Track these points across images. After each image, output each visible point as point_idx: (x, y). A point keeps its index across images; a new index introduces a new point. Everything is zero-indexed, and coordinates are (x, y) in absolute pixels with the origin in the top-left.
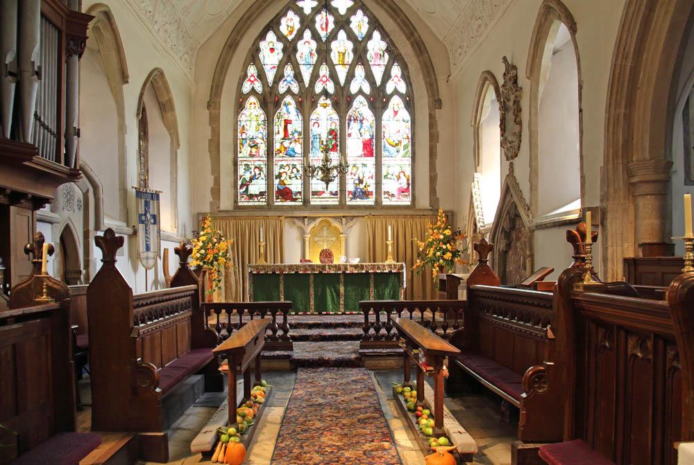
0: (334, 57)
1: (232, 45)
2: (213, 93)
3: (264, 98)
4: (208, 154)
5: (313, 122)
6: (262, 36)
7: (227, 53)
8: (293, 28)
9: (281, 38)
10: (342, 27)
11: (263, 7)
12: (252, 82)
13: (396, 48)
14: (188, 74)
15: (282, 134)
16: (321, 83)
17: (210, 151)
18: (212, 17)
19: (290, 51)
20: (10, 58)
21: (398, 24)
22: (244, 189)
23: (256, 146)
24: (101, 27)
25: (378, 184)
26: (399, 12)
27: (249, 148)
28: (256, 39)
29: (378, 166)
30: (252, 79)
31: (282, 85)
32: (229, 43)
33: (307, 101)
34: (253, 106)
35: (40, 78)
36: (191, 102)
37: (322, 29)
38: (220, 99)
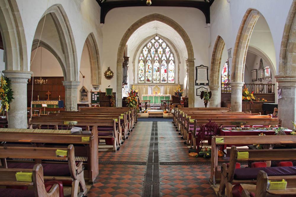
0: (159, 52)
1: (137, 50)
6: (144, 48)
9: (147, 48)
15: (148, 68)
19: (149, 51)
25: (167, 79)
29: (168, 75)
33: (153, 61)
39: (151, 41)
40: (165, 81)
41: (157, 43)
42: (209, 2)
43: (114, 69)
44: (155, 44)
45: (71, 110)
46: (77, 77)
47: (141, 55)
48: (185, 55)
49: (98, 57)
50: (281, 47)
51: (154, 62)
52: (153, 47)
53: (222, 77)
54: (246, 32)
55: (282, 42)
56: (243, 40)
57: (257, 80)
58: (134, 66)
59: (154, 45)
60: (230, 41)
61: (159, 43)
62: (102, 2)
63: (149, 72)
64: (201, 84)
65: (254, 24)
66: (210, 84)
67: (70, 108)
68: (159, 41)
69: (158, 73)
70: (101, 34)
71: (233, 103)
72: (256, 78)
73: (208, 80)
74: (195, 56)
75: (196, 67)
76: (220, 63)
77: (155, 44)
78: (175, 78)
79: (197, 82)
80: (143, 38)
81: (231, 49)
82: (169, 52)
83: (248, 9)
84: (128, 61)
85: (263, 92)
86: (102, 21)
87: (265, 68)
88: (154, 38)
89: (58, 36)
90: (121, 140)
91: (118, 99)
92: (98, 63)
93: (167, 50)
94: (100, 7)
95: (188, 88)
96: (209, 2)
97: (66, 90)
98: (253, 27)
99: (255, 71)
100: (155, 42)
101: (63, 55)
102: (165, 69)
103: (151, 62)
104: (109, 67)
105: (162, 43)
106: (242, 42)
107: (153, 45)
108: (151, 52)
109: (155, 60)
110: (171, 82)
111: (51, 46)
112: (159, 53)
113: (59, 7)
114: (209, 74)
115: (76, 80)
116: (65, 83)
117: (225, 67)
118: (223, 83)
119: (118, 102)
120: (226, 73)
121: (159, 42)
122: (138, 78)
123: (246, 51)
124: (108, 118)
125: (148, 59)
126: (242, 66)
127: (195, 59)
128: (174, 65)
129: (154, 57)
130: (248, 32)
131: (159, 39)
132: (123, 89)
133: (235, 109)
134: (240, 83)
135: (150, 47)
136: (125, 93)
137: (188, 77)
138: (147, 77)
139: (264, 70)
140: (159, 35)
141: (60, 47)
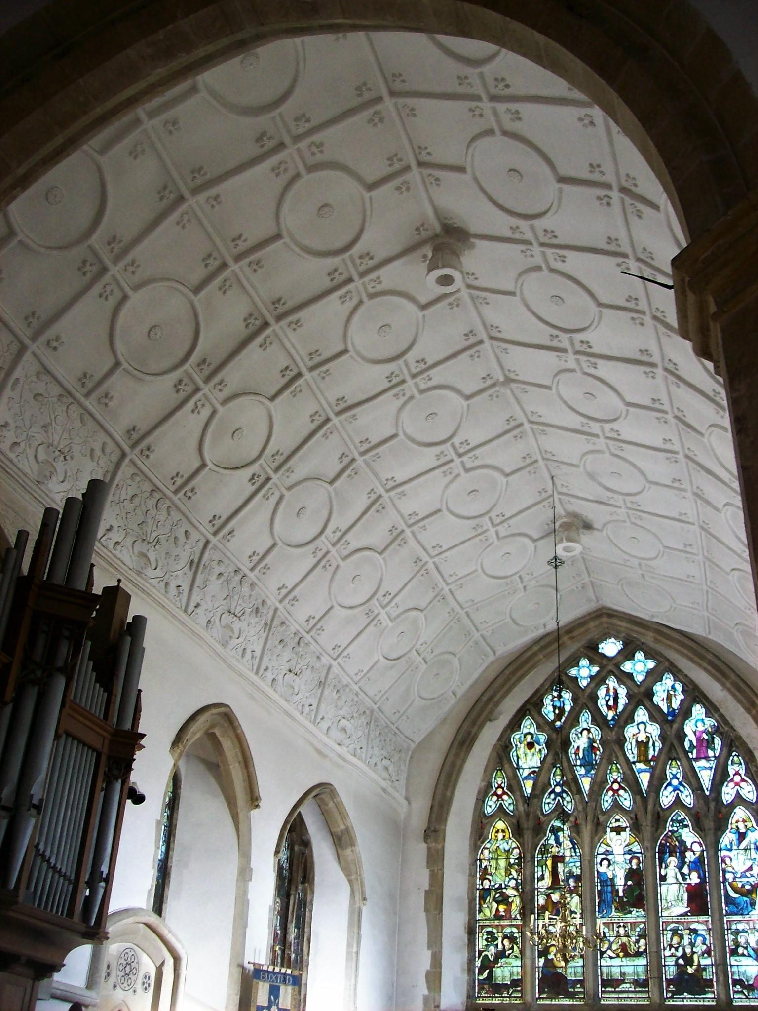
0: (631, 751)
1: (463, 742)
2: (434, 815)
3: (518, 822)
4: (423, 915)
5: (600, 857)
6: (515, 725)
7: (457, 755)
8: (562, 710)
9: (543, 724)
10: (585, 706)
11: (512, 682)
12: (499, 797)
13: (732, 728)
14: (390, 790)
15: (548, 881)
16: (495, 798)
17: (427, 910)
18: (429, 702)
19: (558, 743)
20: (8, 791)
21: (729, 690)
22: (485, 974)
23: (504, 900)
24: (217, 734)
25: (722, 966)
26: (727, 671)
27: (495, 905)
28: (505, 730)
29: (719, 931)
30: (500, 792)
31: (548, 801)
32: (460, 737)
33: (591, 823)
34: (500, 835)
35: (39, 813)
36: (396, 830)
37: (609, 708)
38: (446, 825)
41: (612, 682)
44: (602, 692)
47: (499, 780)
59: (594, 698)
61: (626, 678)
68: (627, 667)
88: (592, 652)
100: (598, 680)
105: (654, 676)
107: (586, 700)
108: (572, 751)
109: (608, 813)
112: (631, 758)
121: (630, 676)
124: (59, 522)
129: (599, 786)
131: (627, 653)
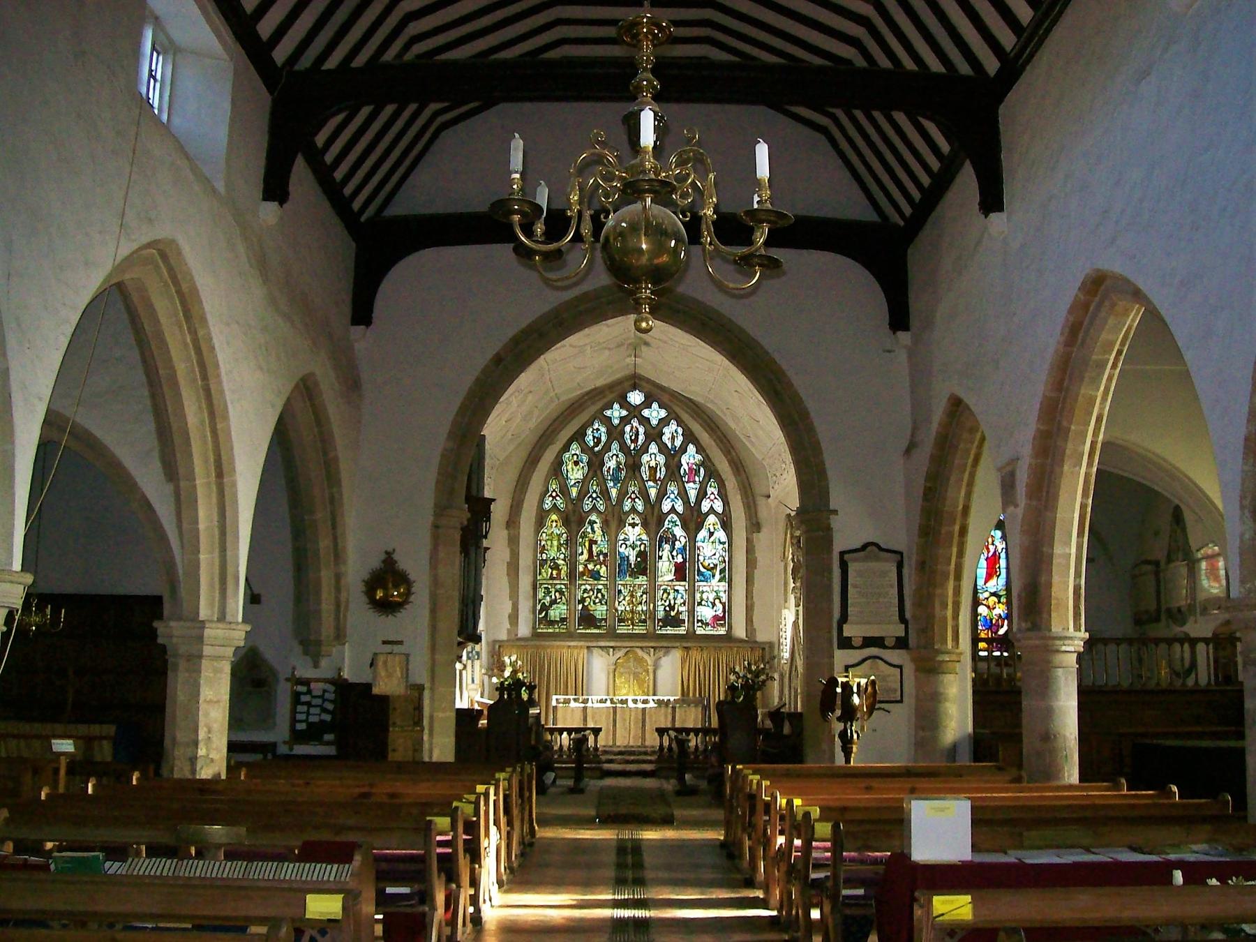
9: (585, 449)
15: (585, 556)
19: (596, 464)
25: (692, 612)
29: (692, 591)
33: (615, 520)
39: (608, 413)
40: (677, 622)
42: (902, 223)
43: (415, 564)
44: (628, 428)
45: (194, 771)
46: (230, 602)
48: (783, 486)
49: (337, 496)
50: (1245, 464)
51: (621, 524)
52: (615, 446)
53: (976, 603)
54: (1086, 380)
55: (1246, 439)
56: (1071, 423)
57: (1157, 620)
58: (513, 542)
60: (1008, 426)
61: (645, 421)
62: (363, 219)
63: (596, 576)
64: (868, 642)
65: (1123, 344)
66: (912, 641)
67: (193, 760)
68: (646, 413)
69: (642, 580)
70: (352, 384)
71: (1029, 742)
72: (1153, 607)
73: (903, 619)
74: (837, 497)
75: (842, 554)
76: (963, 531)
77: (628, 428)
78: (728, 609)
79: (848, 631)
80: (563, 398)
81: (1014, 461)
82: (697, 473)
83: (1087, 275)
84: (489, 519)
85: (1190, 682)
86: (362, 314)
87: (1199, 556)
89: (146, 393)
90: (464, 924)
91: (431, 717)
92: (334, 527)
93: (690, 457)
94: (354, 245)
95: (800, 663)
96: (902, 223)
97: (176, 670)
98: (1117, 359)
99: (1150, 568)
100: (624, 421)
101: (169, 488)
102: (680, 559)
103: (605, 524)
104: (390, 550)
105: (664, 422)
106: (1069, 430)
107: (615, 433)
110: (709, 631)
111: (98, 433)
113: (164, 256)
114: (907, 591)
115: (229, 618)
116: (170, 631)
117: (992, 548)
118: (983, 635)
119: (431, 734)
120: (997, 584)
122: (535, 606)
123: (1087, 475)
125: (587, 508)
126: (1073, 550)
127: (835, 512)
128: (724, 538)
129: (622, 495)
130: (1096, 381)
131: (647, 404)
132: (458, 666)
133: (1048, 772)
134: (1066, 638)
135: (596, 445)
136: (472, 689)
137: (797, 605)
138: (582, 601)
139: (1192, 565)
140: (648, 381)
141: (153, 442)
